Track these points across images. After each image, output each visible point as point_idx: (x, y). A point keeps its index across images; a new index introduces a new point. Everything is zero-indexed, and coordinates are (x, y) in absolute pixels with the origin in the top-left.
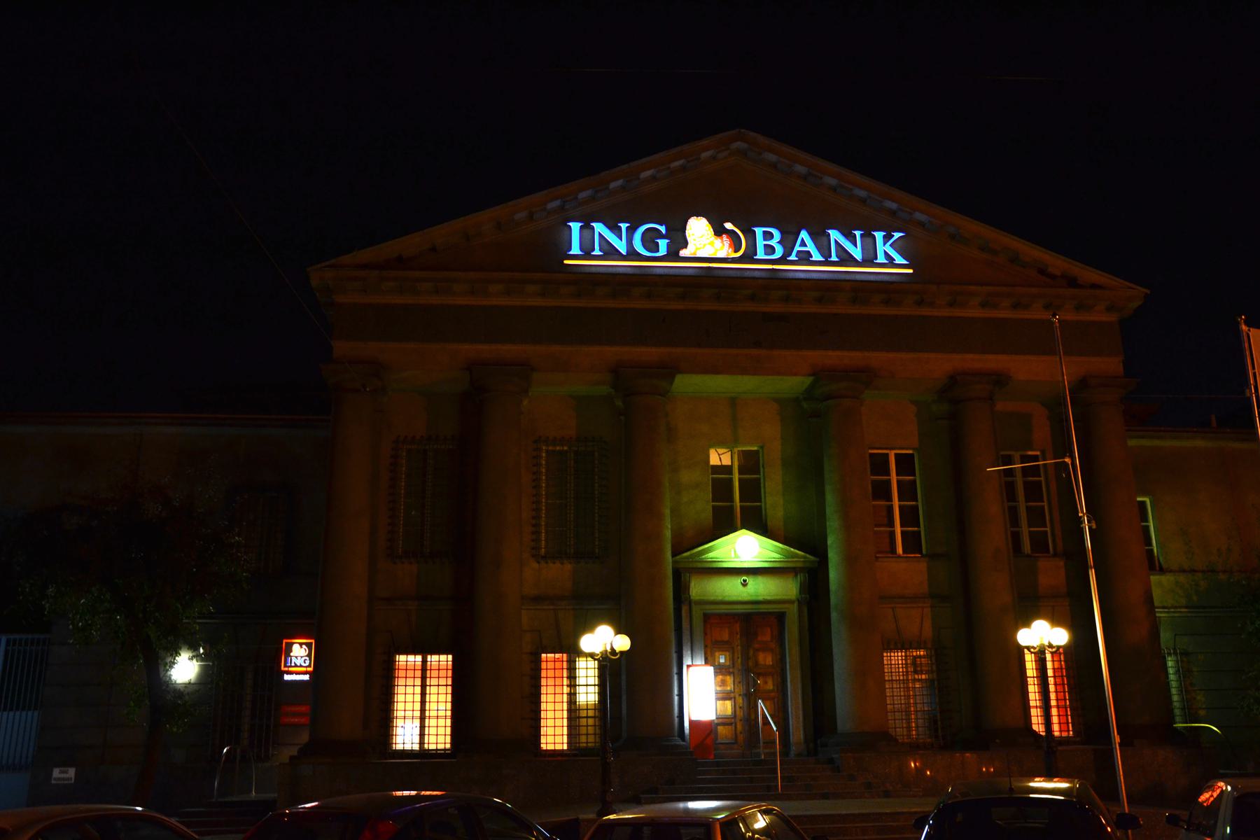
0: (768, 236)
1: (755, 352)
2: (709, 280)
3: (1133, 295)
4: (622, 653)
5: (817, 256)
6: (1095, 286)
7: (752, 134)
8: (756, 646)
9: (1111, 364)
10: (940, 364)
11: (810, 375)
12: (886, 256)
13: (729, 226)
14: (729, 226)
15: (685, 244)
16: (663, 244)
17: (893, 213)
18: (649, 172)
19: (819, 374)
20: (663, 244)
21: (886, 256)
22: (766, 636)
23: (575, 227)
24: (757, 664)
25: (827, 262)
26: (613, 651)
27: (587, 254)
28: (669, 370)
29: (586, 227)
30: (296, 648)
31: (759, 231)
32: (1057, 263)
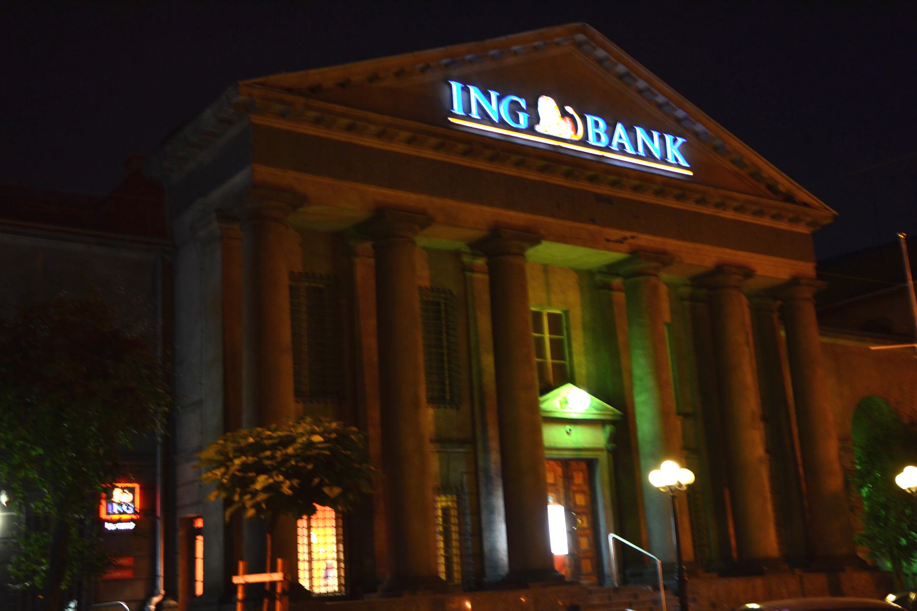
0: (597, 124)
1: (591, 227)
2: (554, 158)
3: (825, 213)
4: (689, 486)
5: (629, 149)
6: (805, 205)
7: (593, 30)
8: (574, 488)
9: (807, 268)
10: (706, 255)
11: (628, 253)
12: (668, 155)
13: (569, 109)
14: (569, 109)
15: (538, 122)
16: (523, 118)
17: (679, 121)
18: (520, 44)
19: (636, 253)
20: (523, 118)
21: (668, 155)
22: (579, 479)
23: (456, 87)
24: (575, 504)
25: (637, 156)
26: (680, 485)
27: (468, 117)
28: (534, 237)
29: (466, 90)
30: (119, 495)
31: (590, 119)
32: (785, 182)
